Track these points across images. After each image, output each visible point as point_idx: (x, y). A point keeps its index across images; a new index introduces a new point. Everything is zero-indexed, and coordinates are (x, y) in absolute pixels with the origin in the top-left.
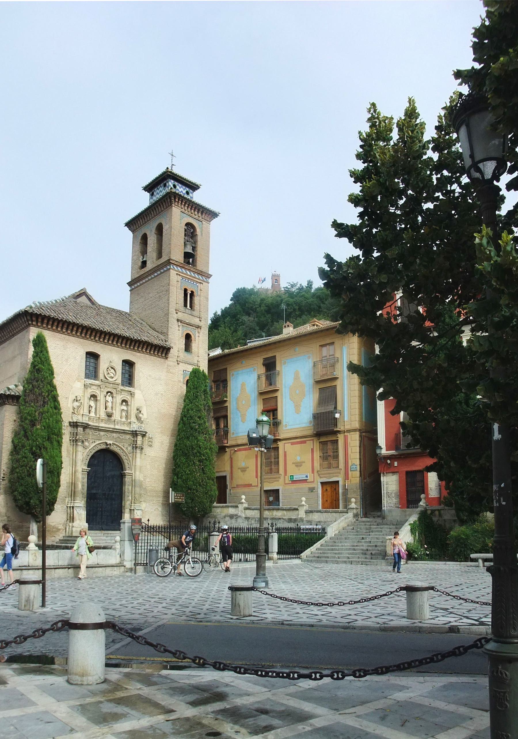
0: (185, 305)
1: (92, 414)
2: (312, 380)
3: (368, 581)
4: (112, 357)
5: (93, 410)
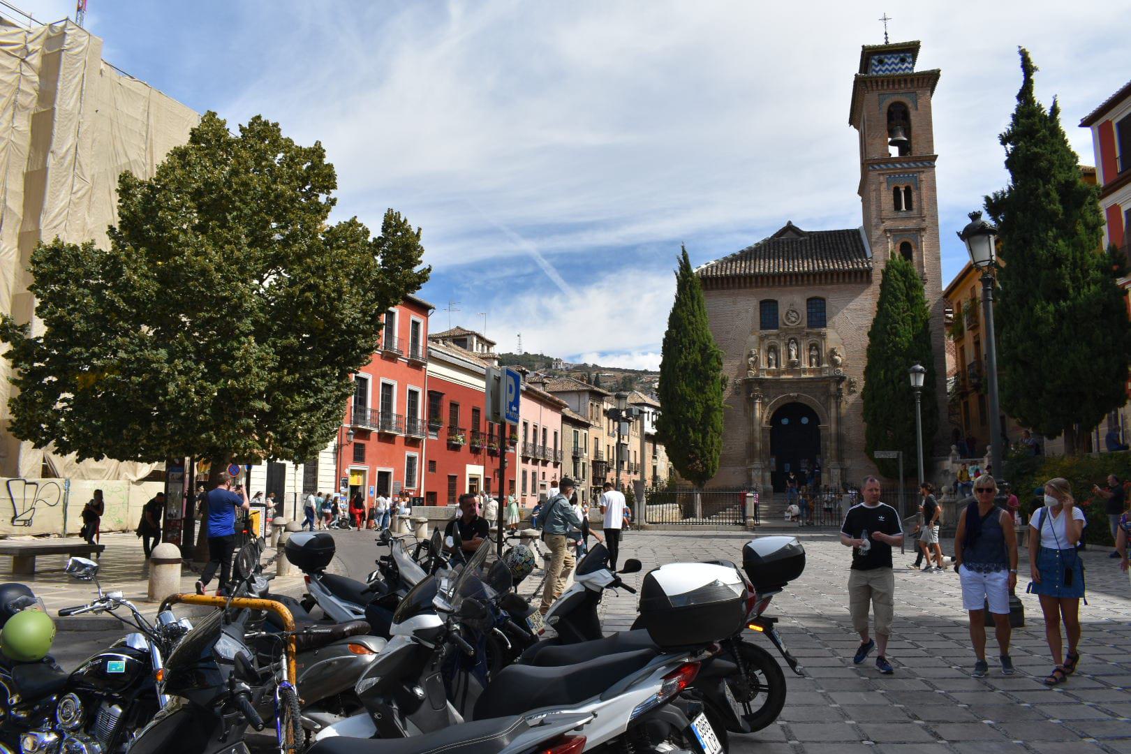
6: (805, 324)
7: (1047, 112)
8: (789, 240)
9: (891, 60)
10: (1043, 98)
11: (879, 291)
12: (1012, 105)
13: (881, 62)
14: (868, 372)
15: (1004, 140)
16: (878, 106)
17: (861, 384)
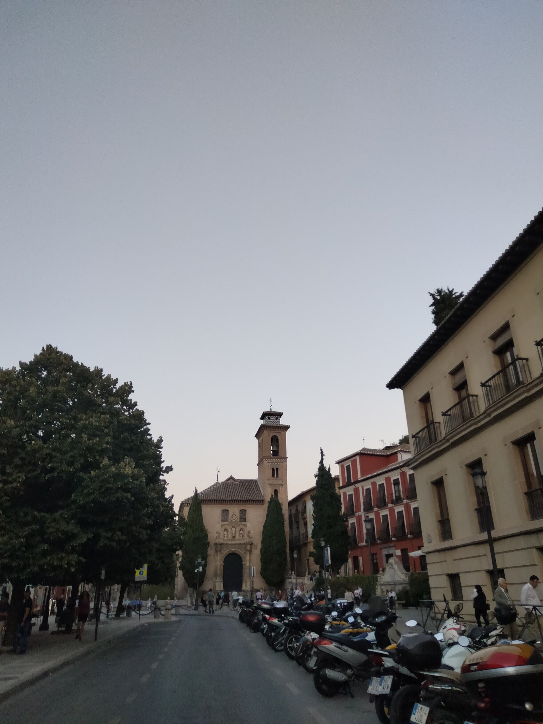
0: (273, 476)
1: (226, 538)
2: (428, 638)
3: (417, 533)
4: (234, 510)
5: (226, 536)
6: (239, 520)
7: (327, 469)
8: (231, 483)
9: (273, 418)
10: (326, 465)
11: (267, 509)
12: (318, 465)
13: (269, 418)
14: (263, 541)
15: (316, 476)
16: (268, 435)
17: (259, 546)
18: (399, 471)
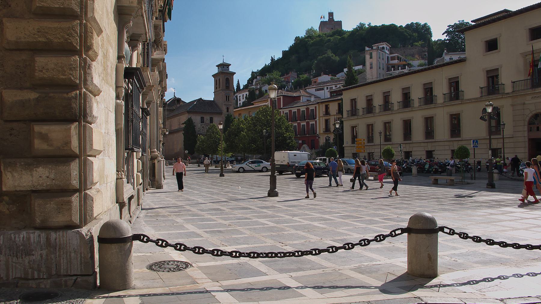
18: (306, 107)
